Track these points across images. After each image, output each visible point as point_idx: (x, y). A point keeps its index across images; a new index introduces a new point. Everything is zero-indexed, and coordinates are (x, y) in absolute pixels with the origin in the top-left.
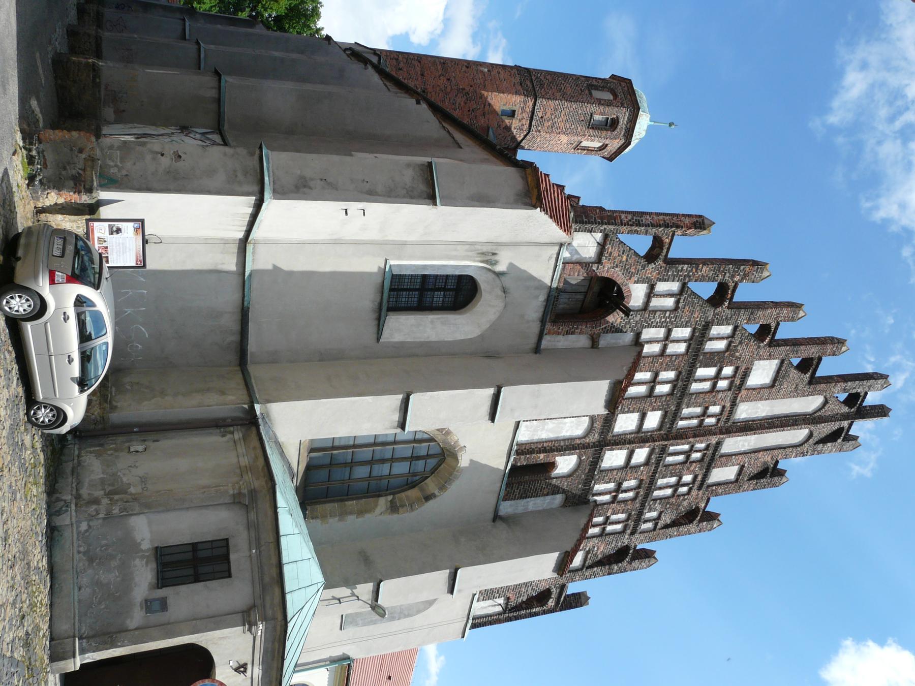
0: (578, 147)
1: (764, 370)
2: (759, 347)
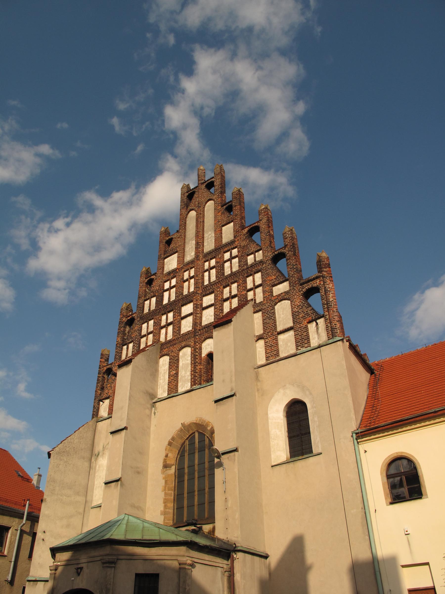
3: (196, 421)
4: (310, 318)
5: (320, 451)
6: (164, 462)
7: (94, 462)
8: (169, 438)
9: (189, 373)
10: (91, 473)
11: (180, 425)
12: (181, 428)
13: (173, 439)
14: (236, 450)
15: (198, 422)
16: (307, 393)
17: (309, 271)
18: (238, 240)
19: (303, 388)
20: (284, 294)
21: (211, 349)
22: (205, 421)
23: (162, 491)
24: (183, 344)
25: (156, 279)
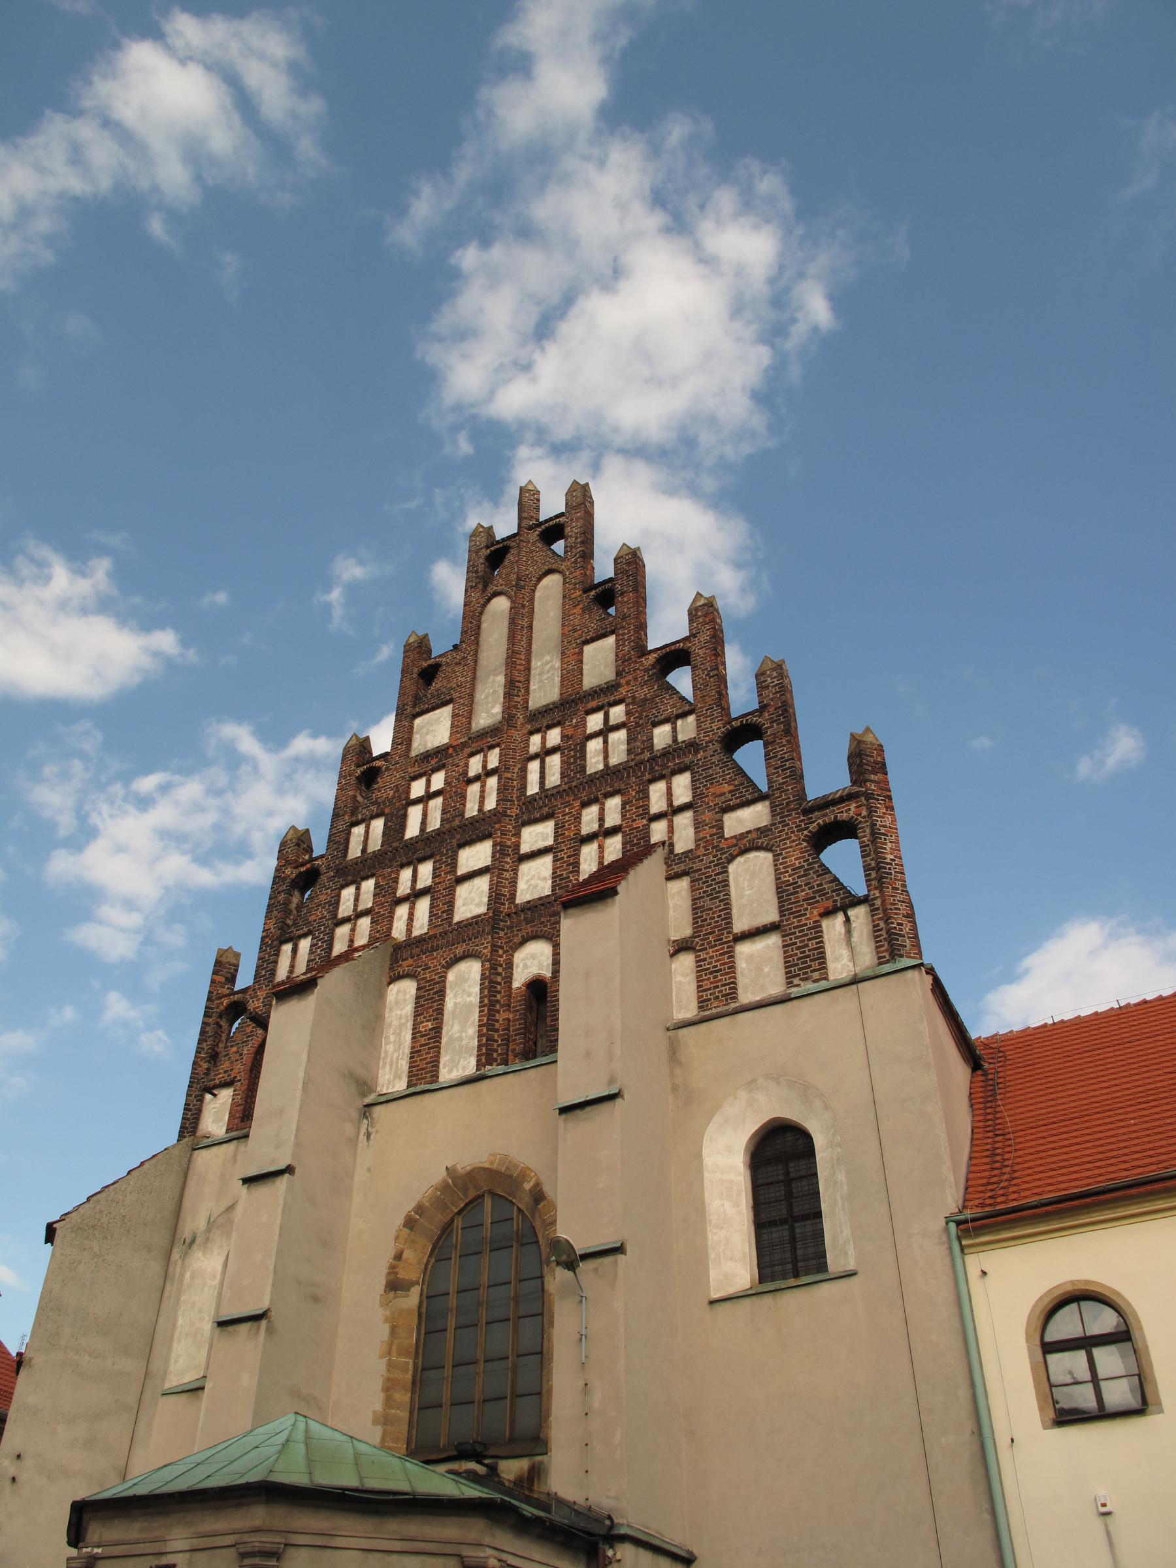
0: (618, 1499)
1: (427, 734)
2: (387, 769)
3: (492, 1163)
4: (829, 904)
5: (851, 1266)
6: (389, 1274)
7: (179, 1262)
8: (408, 1206)
9: (472, 1031)
10: (166, 1294)
11: (444, 1173)
12: (445, 1181)
13: (419, 1209)
14: (619, 1250)
15: (495, 1166)
16: (818, 1103)
17: (825, 776)
18: (628, 683)
19: (805, 1091)
20: (754, 835)
21: (540, 966)
22: (516, 1166)
23: (382, 1357)
24: (459, 950)
25: (387, 769)
